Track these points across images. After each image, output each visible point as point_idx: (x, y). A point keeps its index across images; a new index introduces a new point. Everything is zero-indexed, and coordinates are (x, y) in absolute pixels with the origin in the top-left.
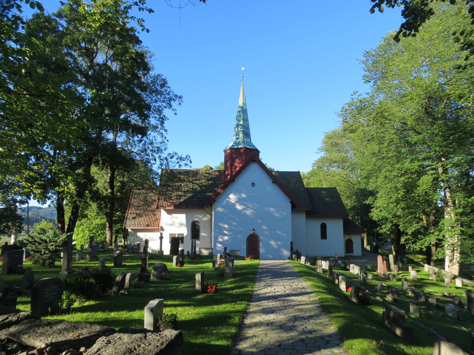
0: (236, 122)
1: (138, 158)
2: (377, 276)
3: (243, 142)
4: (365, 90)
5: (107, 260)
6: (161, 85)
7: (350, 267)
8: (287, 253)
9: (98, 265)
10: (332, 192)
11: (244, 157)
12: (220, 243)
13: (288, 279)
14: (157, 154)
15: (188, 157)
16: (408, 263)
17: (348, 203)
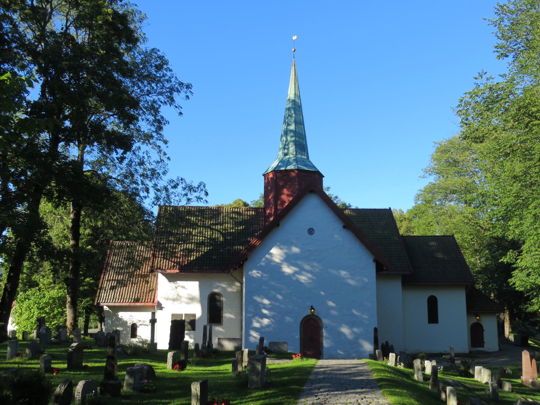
1: (119, 187)
2: (521, 385)
3: (296, 160)
4: (499, 70)
5: (54, 357)
6: (156, 66)
7: (474, 370)
8: (368, 347)
9: (38, 366)
10: (447, 243)
11: (295, 184)
12: (256, 329)
13: (356, 393)
14: (150, 181)
15: (202, 186)
17: (475, 261)
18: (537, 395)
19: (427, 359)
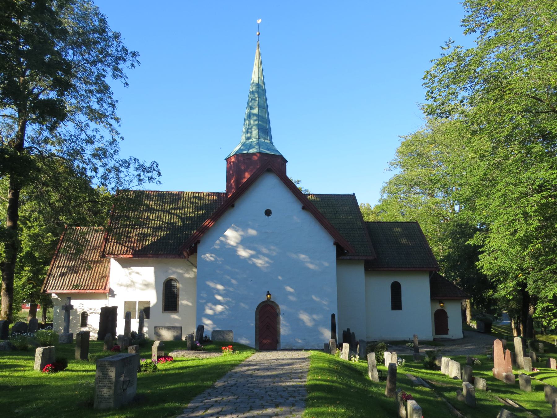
0: (248, 111)
3: (258, 144)
7: (440, 362)
10: (412, 229)
11: (257, 168)
12: (209, 317)
16: (546, 351)
17: (439, 250)
18: (515, 393)
19: (387, 351)
